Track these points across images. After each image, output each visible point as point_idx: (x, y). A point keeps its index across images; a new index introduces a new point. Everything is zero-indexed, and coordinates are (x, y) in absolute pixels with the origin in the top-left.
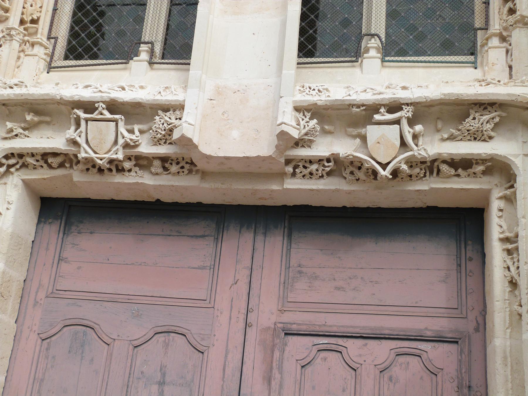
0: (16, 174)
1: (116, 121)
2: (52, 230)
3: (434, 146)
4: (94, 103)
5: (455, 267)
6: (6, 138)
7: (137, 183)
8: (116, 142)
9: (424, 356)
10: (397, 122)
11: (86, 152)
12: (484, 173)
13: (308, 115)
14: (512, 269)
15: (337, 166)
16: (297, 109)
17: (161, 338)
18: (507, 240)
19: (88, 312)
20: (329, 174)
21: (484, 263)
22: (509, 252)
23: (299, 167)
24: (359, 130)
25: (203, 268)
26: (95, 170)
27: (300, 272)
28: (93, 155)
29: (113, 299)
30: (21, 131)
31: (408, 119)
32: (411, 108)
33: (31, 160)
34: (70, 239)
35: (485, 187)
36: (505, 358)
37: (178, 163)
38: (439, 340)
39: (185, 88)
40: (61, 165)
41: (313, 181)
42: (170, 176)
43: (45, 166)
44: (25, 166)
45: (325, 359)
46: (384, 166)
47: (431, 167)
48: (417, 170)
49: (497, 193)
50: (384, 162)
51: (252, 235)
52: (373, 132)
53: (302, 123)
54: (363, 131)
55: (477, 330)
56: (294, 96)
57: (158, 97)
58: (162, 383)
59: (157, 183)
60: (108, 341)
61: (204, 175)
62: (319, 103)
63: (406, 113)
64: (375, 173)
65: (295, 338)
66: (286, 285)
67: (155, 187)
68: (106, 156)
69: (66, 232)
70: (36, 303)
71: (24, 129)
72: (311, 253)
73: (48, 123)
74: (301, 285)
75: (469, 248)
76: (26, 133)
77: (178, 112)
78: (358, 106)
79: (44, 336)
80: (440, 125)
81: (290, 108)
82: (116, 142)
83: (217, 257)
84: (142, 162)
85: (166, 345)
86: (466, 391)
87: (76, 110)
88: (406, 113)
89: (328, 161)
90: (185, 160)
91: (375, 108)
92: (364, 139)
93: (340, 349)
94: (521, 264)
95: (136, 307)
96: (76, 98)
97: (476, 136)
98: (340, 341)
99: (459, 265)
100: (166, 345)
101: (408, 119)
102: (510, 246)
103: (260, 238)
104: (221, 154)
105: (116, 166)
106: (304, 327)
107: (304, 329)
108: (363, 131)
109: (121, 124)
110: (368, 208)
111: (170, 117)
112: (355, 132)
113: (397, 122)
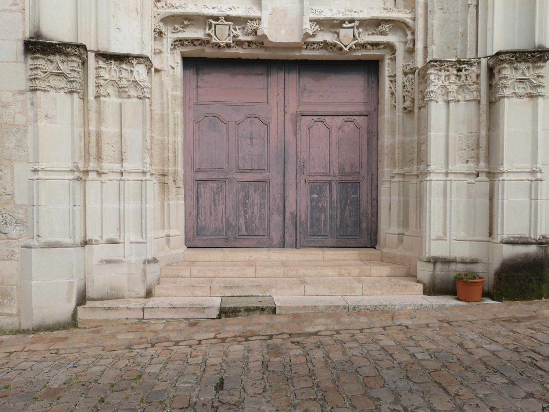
0: (178, 49)
1: (229, 25)
2: (190, 73)
3: (366, 38)
4: (219, 17)
5: (367, 85)
6: (173, 33)
7: (236, 53)
8: (229, 35)
9: (355, 122)
10: (352, 27)
11: (215, 40)
12: (383, 48)
13: (315, 23)
14: (393, 88)
15: (326, 45)
16: (311, 21)
17: (249, 120)
18: (390, 76)
19: (215, 110)
20: (321, 48)
21: (378, 84)
22: (391, 81)
23: (308, 45)
24: (335, 30)
25: (263, 89)
26: (217, 47)
27: (305, 89)
28: (219, 41)
29: (224, 104)
30: (181, 29)
31: (357, 26)
32: (358, 22)
33: (186, 43)
34: (199, 77)
35: (383, 54)
36: (388, 122)
37: (255, 44)
38: (361, 115)
39: (261, 10)
40: (200, 44)
41: (314, 51)
42: (251, 50)
43: (192, 45)
44: (182, 45)
45: (317, 125)
46: (346, 47)
47: (363, 46)
48: (358, 47)
49: (387, 57)
50: (346, 45)
51: (283, 73)
52: (342, 32)
53: (313, 27)
54: (337, 30)
55: (375, 110)
56: (309, 15)
57: (248, 14)
58: (251, 138)
59: (246, 52)
60: (226, 122)
61: (266, 48)
62: (320, 18)
63: (356, 24)
64: (341, 49)
65: (305, 117)
66: (300, 95)
67: (243, 54)
68: (225, 41)
69: (198, 74)
70: (190, 107)
71: (183, 28)
72: (308, 81)
73: (193, 24)
74: (306, 95)
75: (373, 77)
76: (184, 30)
77: (257, 21)
78: (337, 20)
79: (196, 122)
80: (368, 28)
81: (308, 21)
82: (229, 35)
83: (269, 83)
84: (238, 43)
85: (251, 123)
86: (371, 134)
87: (210, 20)
88: (356, 24)
89: (322, 43)
90: (261, 42)
91: (343, 21)
92: (338, 34)
93: (323, 120)
94: (396, 86)
95: (236, 107)
96: (211, 14)
97: (383, 33)
98: (323, 117)
99: (369, 84)
100: (251, 123)
101: (357, 26)
102: (392, 79)
103: (287, 75)
104: (278, 41)
105: (228, 46)
106: (309, 113)
107: (309, 113)
108: (337, 30)
109: (231, 27)
110: (333, 61)
111: (254, 24)
112: (334, 30)
113: (352, 27)
